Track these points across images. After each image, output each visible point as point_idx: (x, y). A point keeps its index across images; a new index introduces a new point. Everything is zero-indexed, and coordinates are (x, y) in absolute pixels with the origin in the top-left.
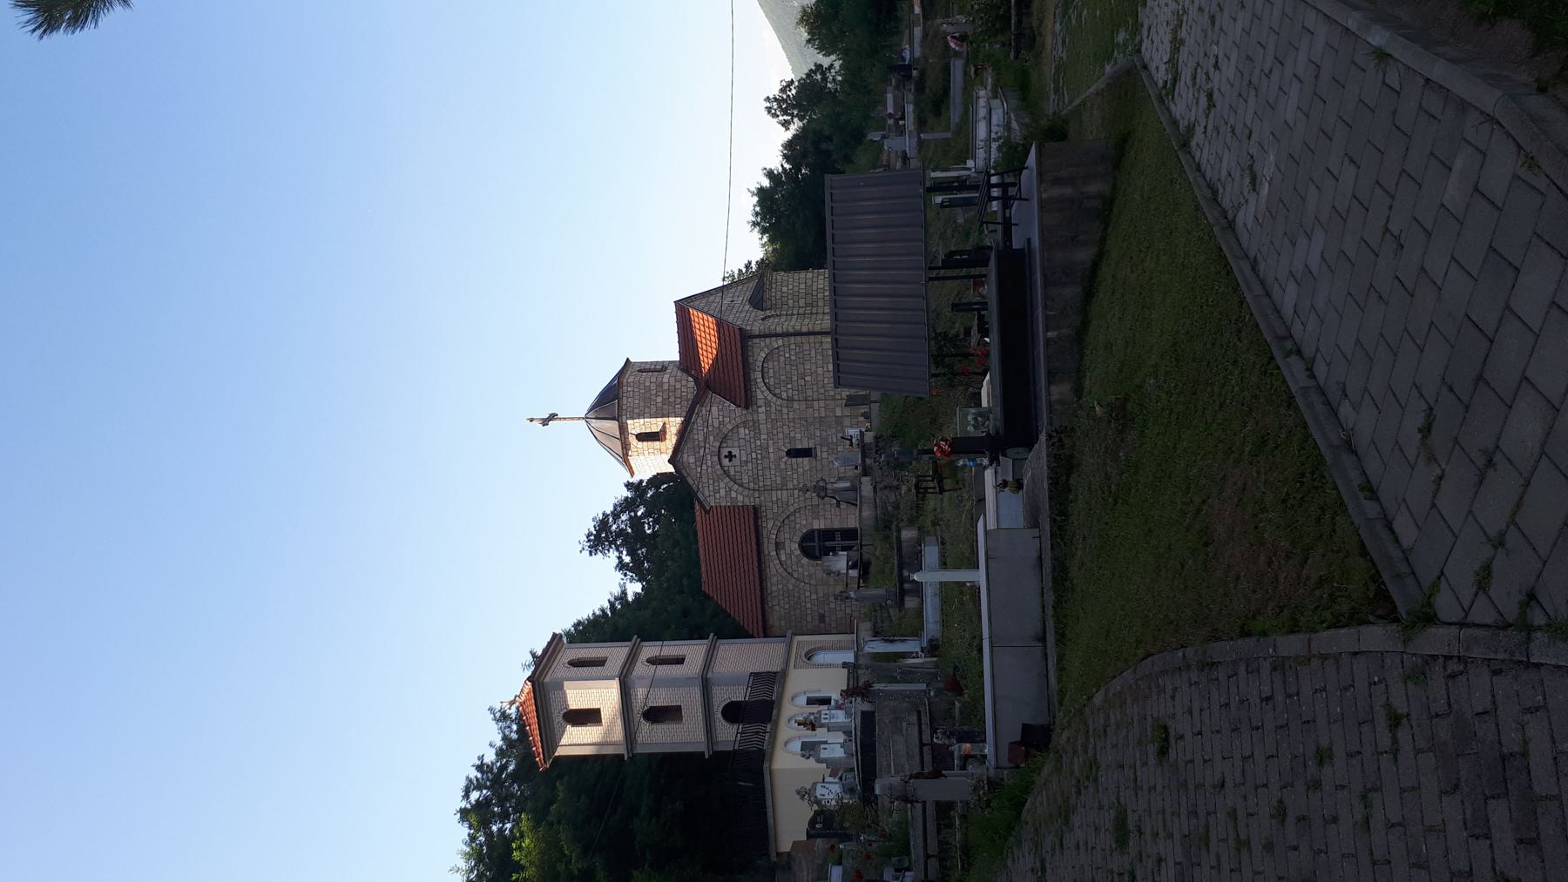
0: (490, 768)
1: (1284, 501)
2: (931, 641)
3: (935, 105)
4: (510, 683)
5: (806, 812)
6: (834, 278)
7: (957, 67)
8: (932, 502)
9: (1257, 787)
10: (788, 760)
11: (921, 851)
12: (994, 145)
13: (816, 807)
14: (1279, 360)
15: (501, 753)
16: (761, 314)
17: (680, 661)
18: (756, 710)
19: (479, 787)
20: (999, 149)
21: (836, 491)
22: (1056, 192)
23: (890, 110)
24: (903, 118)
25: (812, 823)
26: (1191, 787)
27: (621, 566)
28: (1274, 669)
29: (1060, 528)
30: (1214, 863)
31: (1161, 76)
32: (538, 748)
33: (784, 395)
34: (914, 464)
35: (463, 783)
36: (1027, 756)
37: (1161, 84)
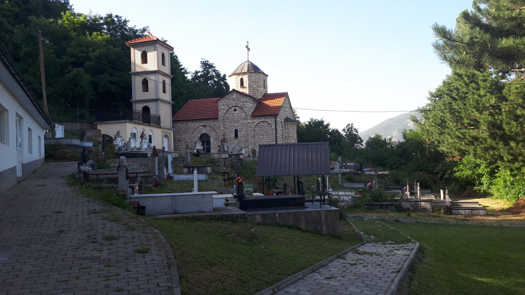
0: (125, 25)
1: (225, 289)
2: (172, 177)
3: (349, 178)
4: (156, 32)
5: (112, 135)
6: (295, 145)
7: (362, 185)
8: (220, 177)
9: (128, 282)
10: (129, 129)
11: (99, 173)
12: (337, 197)
13: (114, 137)
14: (271, 287)
15: (131, 29)
16: (283, 121)
17: (164, 91)
18: (147, 118)
19: (118, 21)
20: (336, 198)
21: (224, 146)
22: (323, 216)
23: (348, 164)
24: (345, 168)
25: (108, 136)
26: (127, 261)
27: (197, 72)
28: (169, 287)
29: (213, 218)
30: (101, 269)
31: (361, 249)
32: (133, 41)
33: (256, 129)
34: (232, 171)
35: (120, 15)
36: (135, 208)
37: (358, 249)
